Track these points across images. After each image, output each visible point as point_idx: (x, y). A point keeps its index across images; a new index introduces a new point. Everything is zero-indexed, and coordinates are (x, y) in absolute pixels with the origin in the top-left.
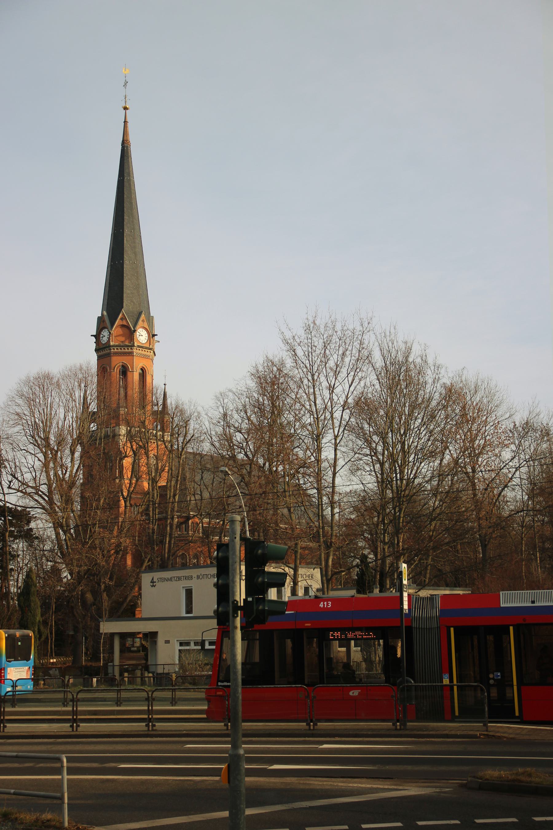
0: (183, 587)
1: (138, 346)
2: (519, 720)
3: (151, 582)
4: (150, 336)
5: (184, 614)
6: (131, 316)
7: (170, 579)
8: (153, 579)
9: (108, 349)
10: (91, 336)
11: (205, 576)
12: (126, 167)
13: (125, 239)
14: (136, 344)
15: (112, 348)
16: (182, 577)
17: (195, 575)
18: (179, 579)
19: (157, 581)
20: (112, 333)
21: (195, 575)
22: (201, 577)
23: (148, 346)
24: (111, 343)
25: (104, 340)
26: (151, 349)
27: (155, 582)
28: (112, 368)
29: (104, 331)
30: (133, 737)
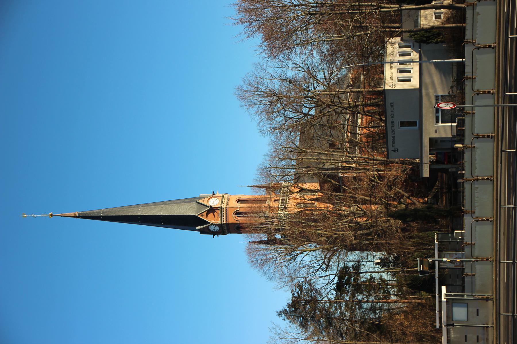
0: (399, 128)
1: (221, 204)
2: (472, 298)
3: (395, 152)
4: (214, 197)
5: (417, 127)
6: (200, 209)
7: (393, 137)
8: (393, 151)
9: (223, 226)
10: (214, 237)
11: (392, 112)
12: (93, 215)
13: (145, 215)
14: (220, 206)
15: (223, 223)
16: (392, 129)
17: (391, 120)
18: (393, 131)
19: (394, 147)
20: (212, 223)
21: (391, 120)
22: (392, 115)
23: (221, 198)
24: (219, 223)
25: (217, 228)
26: (223, 196)
27: (395, 149)
28: (237, 222)
29: (210, 229)
30: (500, 56)
